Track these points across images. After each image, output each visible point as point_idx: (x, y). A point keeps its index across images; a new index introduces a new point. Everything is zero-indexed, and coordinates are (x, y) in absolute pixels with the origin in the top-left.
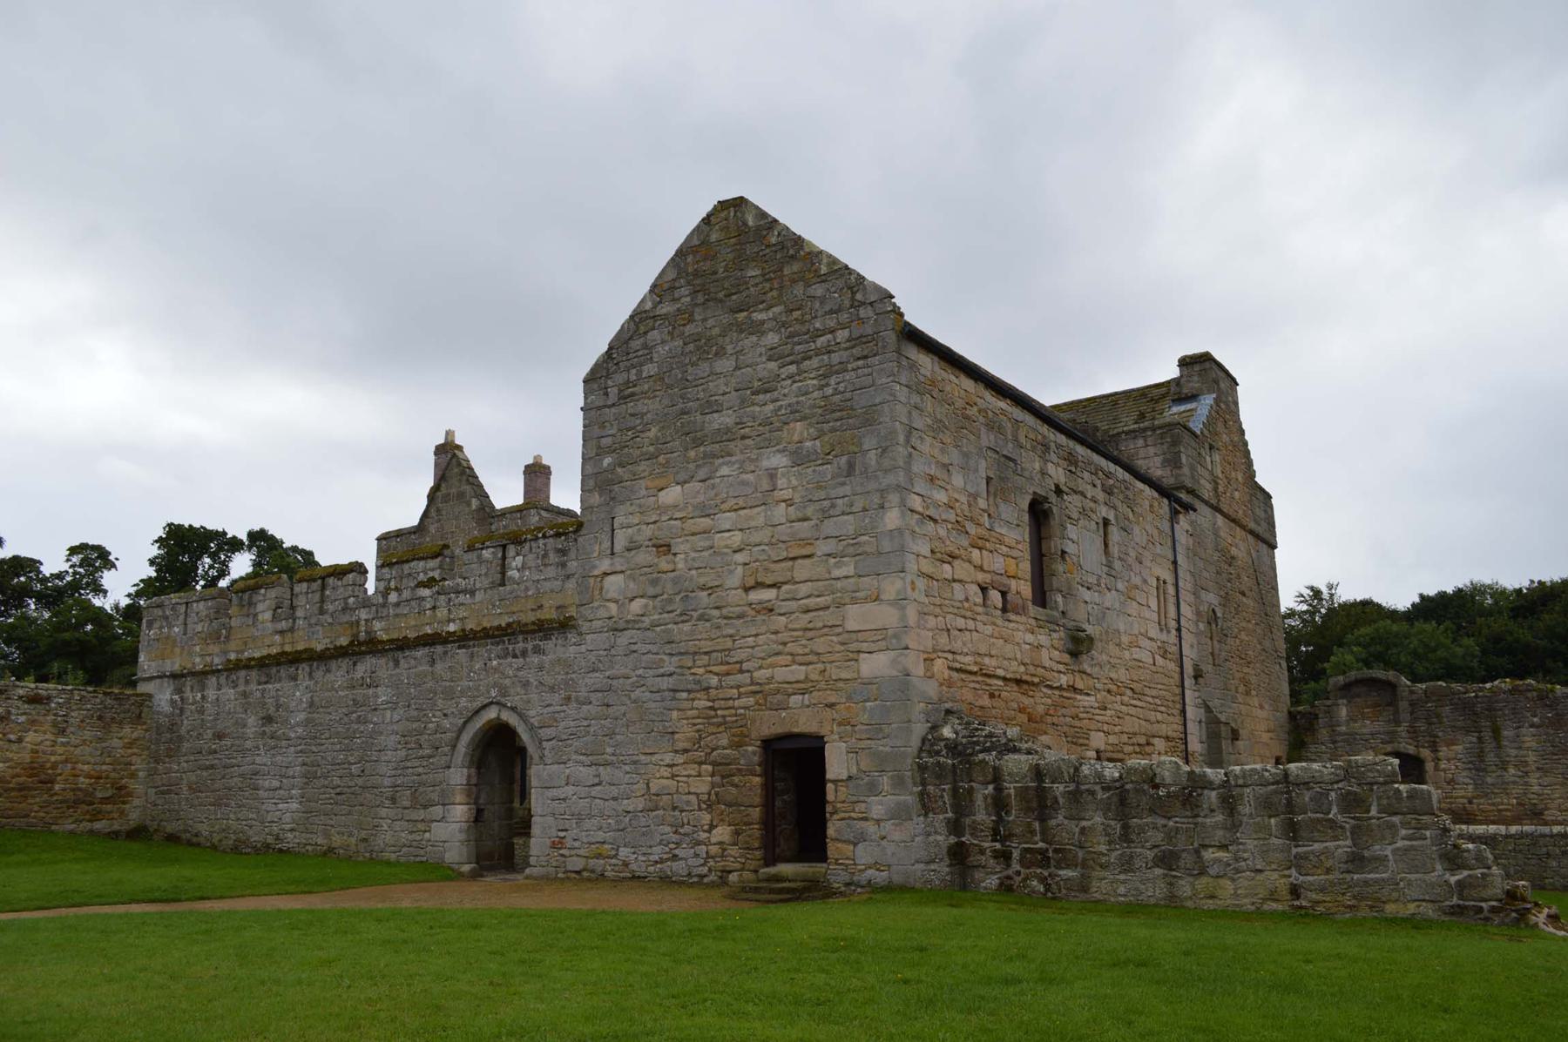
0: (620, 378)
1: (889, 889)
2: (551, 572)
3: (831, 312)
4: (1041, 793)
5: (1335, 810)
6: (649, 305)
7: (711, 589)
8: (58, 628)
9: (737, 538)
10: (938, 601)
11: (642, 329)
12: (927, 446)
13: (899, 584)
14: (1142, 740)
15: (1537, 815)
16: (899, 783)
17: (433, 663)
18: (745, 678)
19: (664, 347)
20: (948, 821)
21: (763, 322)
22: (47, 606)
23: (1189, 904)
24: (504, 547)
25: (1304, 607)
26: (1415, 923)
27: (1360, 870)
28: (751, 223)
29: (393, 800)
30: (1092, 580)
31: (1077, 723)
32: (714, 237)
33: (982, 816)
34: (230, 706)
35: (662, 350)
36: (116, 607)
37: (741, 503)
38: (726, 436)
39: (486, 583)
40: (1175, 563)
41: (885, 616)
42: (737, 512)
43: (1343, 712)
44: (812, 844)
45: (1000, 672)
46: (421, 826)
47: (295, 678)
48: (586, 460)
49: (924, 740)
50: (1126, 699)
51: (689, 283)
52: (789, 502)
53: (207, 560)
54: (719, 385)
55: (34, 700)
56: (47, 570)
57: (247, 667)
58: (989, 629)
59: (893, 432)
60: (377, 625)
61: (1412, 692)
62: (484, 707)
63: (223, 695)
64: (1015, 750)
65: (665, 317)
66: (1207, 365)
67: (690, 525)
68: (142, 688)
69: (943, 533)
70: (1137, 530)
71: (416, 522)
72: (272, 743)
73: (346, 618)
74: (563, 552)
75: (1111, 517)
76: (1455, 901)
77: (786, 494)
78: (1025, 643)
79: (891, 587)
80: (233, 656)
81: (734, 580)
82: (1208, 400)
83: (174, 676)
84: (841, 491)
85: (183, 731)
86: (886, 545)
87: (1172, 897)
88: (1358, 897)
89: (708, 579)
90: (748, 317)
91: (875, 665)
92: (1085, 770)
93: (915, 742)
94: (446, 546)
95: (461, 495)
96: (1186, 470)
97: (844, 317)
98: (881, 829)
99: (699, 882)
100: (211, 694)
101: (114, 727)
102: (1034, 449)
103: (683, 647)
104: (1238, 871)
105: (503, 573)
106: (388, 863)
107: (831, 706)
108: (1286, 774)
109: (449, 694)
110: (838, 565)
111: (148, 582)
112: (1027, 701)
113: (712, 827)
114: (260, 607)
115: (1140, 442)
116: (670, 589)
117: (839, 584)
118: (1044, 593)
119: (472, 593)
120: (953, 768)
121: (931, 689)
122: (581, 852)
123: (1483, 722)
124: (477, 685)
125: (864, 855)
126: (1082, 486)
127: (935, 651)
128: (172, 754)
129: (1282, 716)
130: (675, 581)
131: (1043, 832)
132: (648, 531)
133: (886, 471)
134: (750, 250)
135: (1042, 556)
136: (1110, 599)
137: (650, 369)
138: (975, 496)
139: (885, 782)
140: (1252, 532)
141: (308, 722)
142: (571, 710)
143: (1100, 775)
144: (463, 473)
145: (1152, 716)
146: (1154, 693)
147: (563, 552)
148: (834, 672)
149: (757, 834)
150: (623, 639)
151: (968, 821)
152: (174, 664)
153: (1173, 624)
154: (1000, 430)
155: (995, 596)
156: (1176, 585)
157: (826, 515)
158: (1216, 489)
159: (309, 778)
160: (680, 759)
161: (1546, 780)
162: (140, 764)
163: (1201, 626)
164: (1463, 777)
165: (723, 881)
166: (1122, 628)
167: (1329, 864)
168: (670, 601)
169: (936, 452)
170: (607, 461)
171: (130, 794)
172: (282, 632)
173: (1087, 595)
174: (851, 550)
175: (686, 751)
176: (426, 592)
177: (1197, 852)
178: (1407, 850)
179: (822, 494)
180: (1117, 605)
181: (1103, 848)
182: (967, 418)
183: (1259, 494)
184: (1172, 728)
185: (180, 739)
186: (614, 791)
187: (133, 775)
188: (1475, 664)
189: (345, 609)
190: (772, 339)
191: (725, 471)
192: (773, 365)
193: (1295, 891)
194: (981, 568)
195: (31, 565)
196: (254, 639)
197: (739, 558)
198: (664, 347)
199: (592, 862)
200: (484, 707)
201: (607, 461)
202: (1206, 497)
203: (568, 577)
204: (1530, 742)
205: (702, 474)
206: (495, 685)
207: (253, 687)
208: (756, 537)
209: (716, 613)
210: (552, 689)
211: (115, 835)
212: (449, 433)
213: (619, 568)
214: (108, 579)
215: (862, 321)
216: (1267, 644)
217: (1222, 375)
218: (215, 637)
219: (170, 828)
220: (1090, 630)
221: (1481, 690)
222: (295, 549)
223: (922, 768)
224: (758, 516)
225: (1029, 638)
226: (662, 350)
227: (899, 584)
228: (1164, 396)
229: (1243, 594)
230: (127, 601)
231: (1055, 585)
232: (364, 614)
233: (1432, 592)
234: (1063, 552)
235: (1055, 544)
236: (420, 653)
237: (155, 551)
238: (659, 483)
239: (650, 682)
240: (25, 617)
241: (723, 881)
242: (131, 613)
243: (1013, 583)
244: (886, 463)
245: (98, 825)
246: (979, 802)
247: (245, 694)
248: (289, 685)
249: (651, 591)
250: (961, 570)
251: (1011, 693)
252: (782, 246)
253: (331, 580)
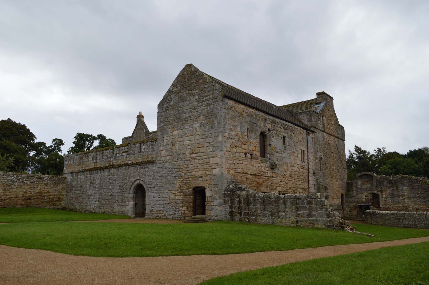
0: (165, 105)
1: (217, 221)
2: (150, 150)
3: (209, 91)
4: (248, 200)
5: (305, 204)
6: (171, 89)
7: (183, 154)
8: (51, 160)
9: (188, 143)
10: (232, 157)
11: (170, 94)
12: (230, 122)
13: (221, 153)
14: (294, 189)
15: (407, 209)
16: (220, 197)
17: (126, 170)
18: (190, 174)
19: (174, 98)
20: (230, 206)
21: (195, 93)
22: (47, 154)
23: (276, 224)
24: (141, 144)
25: (376, 154)
26: (319, 229)
27: (310, 217)
28: (193, 70)
29: (118, 201)
30: (279, 151)
31: (273, 185)
32: (185, 73)
33: (236, 205)
34: (83, 180)
35: (174, 99)
36: (65, 155)
37: (190, 135)
38: (187, 119)
39: (137, 152)
40: (307, 146)
41: (218, 160)
42: (188, 137)
43: (360, 183)
44: (203, 212)
45: (249, 173)
46: (123, 207)
47: (97, 173)
48: (158, 124)
49: (226, 188)
50: (289, 179)
51: (180, 84)
52: (199, 135)
53: (87, 142)
54: (185, 108)
55: (40, 178)
56: (47, 145)
57: (87, 171)
58: (246, 163)
59: (220, 119)
60: (114, 161)
61: (377, 178)
62: (136, 180)
63: (81, 177)
64: (245, 191)
65: (174, 91)
66: (323, 95)
67: (179, 140)
68: (64, 176)
69: (233, 141)
70: (295, 138)
71: (131, 135)
72: (92, 188)
73: (107, 160)
74: (153, 145)
75: (286, 135)
76: (329, 224)
77: (199, 133)
78: (258, 166)
79: (219, 154)
80: (84, 168)
81: (188, 152)
82: (323, 104)
83: (71, 173)
84: (210, 132)
85: (73, 185)
86: (219, 145)
87: (273, 223)
88: (310, 223)
89: (183, 152)
90: (193, 92)
91: (216, 171)
92: (257, 195)
93: (224, 188)
94: (129, 144)
95: (141, 129)
96: (313, 122)
97: (211, 92)
98: (216, 208)
99: (180, 219)
100: (79, 177)
101: (58, 185)
102: (262, 120)
103: (177, 167)
104: (286, 217)
105: (141, 150)
106: (116, 215)
107: (207, 180)
108: (296, 196)
109: (129, 177)
110: (209, 149)
111: (72, 148)
112: (257, 179)
113: (183, 207)
114: (90, 157)
115: (303, 115)
116: (175, 154)
117: (209, 153)
118: (265, 154)
119: (134, 154)
120: (231, 195)
121: (229, 177)
122: (156, 212)
123: (394, 185)
124: (135, 175)
125: (213, 213)
126: (276, 128)
127: (230, 168)
128: (71, 191)
129: (344, 183)
130: (176, 152)
131: (248, 208)
132: (171, 141)
133: (219, 128)
134: (193, 76)
135: (264, 145)
136: (284, 155)
137: (171, 104)
138: (244, 133)
139: (217, 197)
140: (336, 137)
141: (100, 183)
142: (154, 181)
143: (259, 196)
144: (142, 123)
145: (298, 183)
146: (299, 178)
147: (153, 145)
148: (208, 173)
149: (192, 208)
150: (165, 165)
151: (233, 206)
152: (71, 170)
153: (306, 161)
154: (252, 116)
155: (249, 156)
156: (308, 151)
157: (207, 138)
158: (324, 127)
159: (100, 196)
160: (176, 192)
161: (409, 201)
162: (64, 193)
163: (317, 161)
164: (389, 199)
165: (185, 219)
166: (288, 162)
167: (304, 216)
168: (175, 157)
169: (233, 123)
170: (162, 125)
171: (62, 200)
172: (94, 163)
173: (277, 154)
174: (212, 146)
175: (178, 190)
176: (124, 154)
177: (278, 213)
178: (320, 213)
179: (206, 133)
180: (287, 157)
181: (260, 212)
182: (242, 114)
183: (339, 127)
184: (305, 186)
185: (73, 187)
186: (163, 199)
187: (63, 195)
188: (422, 170)
189: (108, 158)
190: (197, 97)
191: (186, 127)
192: (196, 103)
193: (297, 222)
194: (245, 149)
195: (44, 144)
196: (88, 164)
197: (189, 147)
198: (174, 98)
199: (158, 215)
200: (136, 180)
201: (162, 125)
202: (320, 128)
203: (154, 151)
204: (405, 191)
205: (182, 128)
206: (139, 175)
207: (88, 175)
208: (193, 142)
209: (184, 159)
210: (150, 176)
211: (59, 209)
212: (140, 113)
213: (164, 149)
214: (62, 148)
215: (215, 94)
216: (340, 165)
217: (328, 97)
218: (80, 164)
219: (71, 207)
220: (277, 163)
221: (394, 177)
222: (110, 139)
223: (225, 194)
224: (193, 138)
225: (259, 165)
226: (174, 99)
227: (221, 153)
228: (313, 103)
229: (332, 153)
230: (67, 153)
231: (267, 152)
232: (111, 159)
233: (412, 150)
234: (270, 145)
235: (268, 143)
236: (123, 168)
237: (74, 140)
238: (173, 130)
239: (170, 174)
240: (42, 157)
241: (185, 219)
242: (67, 156)
243: (254, 152)
244: (219, 126)
245: (55, 207)
246: (236, 202)
247: (86, 177)
248: (96, 175)
249: (171, 154)
250: (238, 149)
251: (253, 178)
252: (199, 75)
253: (105, 151)
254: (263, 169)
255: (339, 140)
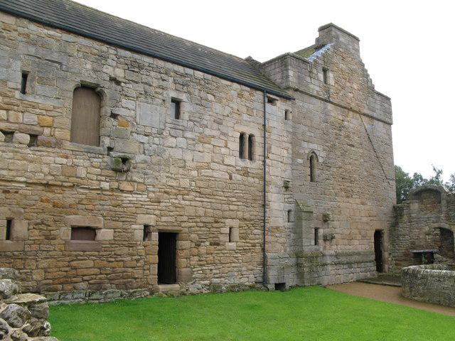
112: (50, 195)
184: (256, 212)
202: (315, 93)
243: (47, 131)
254: (82, 172)
255: (376, 122)
